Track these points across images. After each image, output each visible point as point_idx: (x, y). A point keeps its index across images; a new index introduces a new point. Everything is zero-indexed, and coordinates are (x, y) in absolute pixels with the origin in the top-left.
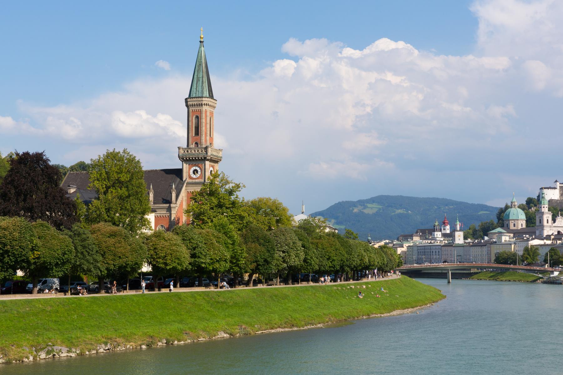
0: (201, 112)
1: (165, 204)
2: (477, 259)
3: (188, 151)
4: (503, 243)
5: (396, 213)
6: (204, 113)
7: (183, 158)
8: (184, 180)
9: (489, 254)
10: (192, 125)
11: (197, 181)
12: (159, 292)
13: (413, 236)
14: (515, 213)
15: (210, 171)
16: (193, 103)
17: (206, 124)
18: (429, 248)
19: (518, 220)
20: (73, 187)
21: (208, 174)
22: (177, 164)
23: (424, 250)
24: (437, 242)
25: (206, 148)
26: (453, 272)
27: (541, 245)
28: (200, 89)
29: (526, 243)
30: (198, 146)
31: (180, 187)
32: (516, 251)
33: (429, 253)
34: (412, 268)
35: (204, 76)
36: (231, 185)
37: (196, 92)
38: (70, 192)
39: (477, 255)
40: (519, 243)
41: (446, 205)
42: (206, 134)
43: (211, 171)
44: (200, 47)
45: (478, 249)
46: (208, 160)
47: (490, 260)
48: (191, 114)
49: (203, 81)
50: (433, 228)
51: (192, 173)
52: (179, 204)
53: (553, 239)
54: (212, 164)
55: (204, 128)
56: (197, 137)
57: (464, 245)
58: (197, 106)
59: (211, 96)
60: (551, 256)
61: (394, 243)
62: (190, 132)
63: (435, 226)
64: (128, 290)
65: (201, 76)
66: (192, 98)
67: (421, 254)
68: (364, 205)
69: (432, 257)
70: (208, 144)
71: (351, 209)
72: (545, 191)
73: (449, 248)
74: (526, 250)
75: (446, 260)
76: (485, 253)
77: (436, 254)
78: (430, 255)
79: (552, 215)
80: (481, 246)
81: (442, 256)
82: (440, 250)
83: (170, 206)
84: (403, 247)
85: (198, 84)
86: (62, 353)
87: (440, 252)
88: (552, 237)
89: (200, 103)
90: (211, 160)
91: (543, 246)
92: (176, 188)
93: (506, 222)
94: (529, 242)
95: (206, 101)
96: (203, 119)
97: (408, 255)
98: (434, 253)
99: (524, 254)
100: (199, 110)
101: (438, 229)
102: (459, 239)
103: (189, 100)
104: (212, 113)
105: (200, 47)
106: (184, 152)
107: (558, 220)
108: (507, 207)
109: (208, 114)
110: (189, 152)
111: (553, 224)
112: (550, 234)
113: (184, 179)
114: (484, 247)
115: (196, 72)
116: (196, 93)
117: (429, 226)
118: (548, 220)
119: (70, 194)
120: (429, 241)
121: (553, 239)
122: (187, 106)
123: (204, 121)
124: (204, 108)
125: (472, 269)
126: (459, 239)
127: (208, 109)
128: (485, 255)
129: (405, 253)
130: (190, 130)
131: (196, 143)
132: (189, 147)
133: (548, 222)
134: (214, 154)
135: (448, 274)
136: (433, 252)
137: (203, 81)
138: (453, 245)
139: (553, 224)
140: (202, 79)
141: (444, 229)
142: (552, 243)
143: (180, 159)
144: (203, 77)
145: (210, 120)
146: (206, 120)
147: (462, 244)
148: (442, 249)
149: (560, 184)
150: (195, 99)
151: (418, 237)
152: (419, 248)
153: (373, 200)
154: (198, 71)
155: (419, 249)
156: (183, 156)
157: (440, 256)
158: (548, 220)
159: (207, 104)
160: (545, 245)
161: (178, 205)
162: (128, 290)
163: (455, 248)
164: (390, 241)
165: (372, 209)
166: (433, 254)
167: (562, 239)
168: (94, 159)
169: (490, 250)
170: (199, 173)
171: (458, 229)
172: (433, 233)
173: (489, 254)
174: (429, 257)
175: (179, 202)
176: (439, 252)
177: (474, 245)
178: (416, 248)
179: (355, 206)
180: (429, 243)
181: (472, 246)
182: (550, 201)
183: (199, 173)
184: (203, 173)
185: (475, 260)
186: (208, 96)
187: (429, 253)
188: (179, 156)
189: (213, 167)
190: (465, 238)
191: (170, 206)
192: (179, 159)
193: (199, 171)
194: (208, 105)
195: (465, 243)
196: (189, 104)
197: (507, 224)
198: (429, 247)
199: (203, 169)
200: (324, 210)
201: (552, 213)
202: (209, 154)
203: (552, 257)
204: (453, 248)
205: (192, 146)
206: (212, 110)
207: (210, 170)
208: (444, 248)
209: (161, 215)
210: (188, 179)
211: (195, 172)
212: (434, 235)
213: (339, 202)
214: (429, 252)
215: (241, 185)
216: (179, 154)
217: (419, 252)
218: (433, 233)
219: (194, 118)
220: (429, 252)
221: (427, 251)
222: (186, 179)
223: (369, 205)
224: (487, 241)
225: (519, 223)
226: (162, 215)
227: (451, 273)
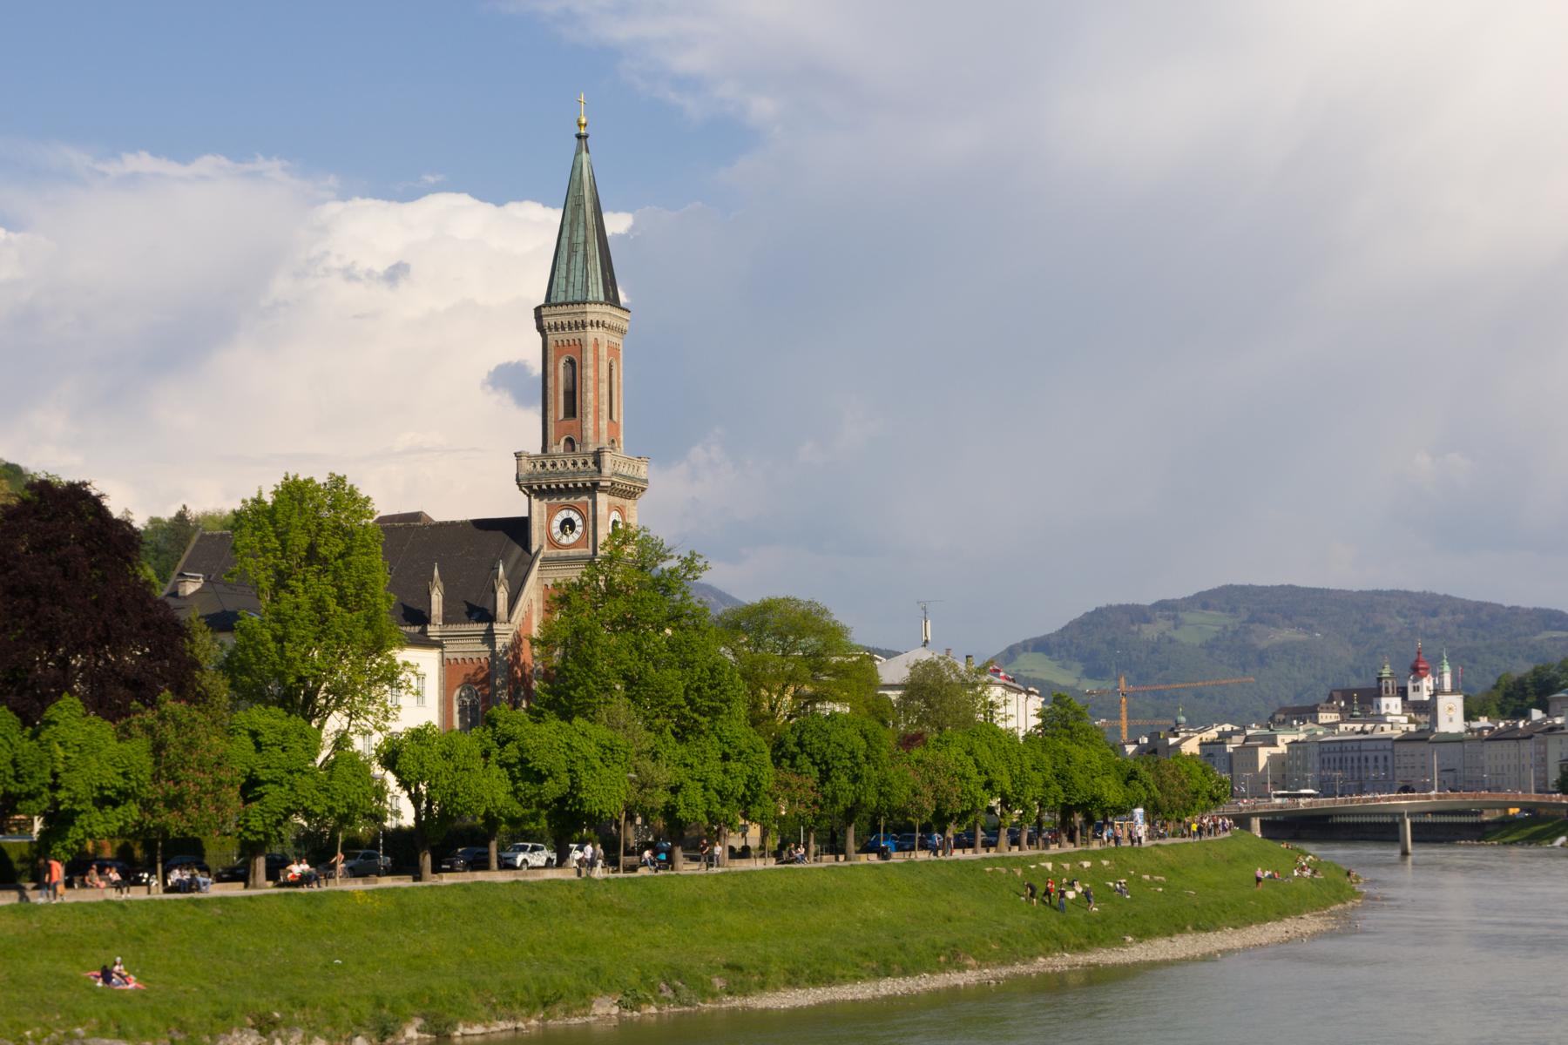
0: (580, 346)
1: (475, 625)
3: (544, 465)
6: (590, 348)
7: (530, 488)
8: (534, 550)
11: (571, 552)
12: (418, 884)
13: (1318, 712)
15: (610, 524)
16: (559, 320)
20: (192, 577)
21: (604, 532)
22: (513, 504)
24: (1382, 729)
25: (597, 457)
26: (1418, 819)
28: (579, 278)
30: (573, 450)
31: (522, 574)
34: (1325, 806)
35: (590, 240)
37: (567, 286)
38: (184, 592)
42: (597, 411)
43: (615, 523)
44: (578, 153)
45: (1509, 748)
46: (604, 490)
47: (1546, 784)
49: (585, 255)
50: (1373, 684)
51: (559, 530)
52: (518, 623)
54: (617, 501)
55: (591, 396)
56: (571, 422)
57: (1465, 736)
58: (570, 328)
59: (612, 299)
61: (1249, 732)
62: (551, 406)
63: (1380, 679)
65: (581, 239)
66: (556, 305)
67: (1332, 766)
69: (1364, 774)
70: (604, 441)
73: (1422, 747)
75: (1408, 784)
77: (1376, 767)
78: (1359, 768)
80: (1517, 739)
81: (1398, 772)
82: (1389, 754)
83: (490, 629)
84: (1275, 744)
85: (573, 262)
87: (1389, 759)
89: (579, 320)
90: (613, 490)
92: (509, 577)
95: (595, 312)
97: (1291, 770)
98: (1371, 763)
100: (577, 342)
101: (1390, 689)
102: (1451, 720)
103: (544, 311)
105: (578, 153)
106: (535, 466)
109: (603, 351)
113: (534, 549)
115: (566, 229)
116: (566, 291)
119: (185, 598)
120: (1358, 727)
122: (540, 328)
123: (590, 372)
124: (592, 334)
125: (1486, 812)
126: (1451, 720)
127: (603, 337)
129: (1283, 764)
130: (551, 400)
131: (570, 441)
132: (549, 452)
134: (624, 473)
135: (1401, 827)
136: (1367, 759)
137: (585, 255)
138: (1431, 738)
141: (1416, 689)
143: (521, 489)
144: (585, 243)
145: (611, 370)
146: (597, 371)
147: (1460, 734)
148: (1396, 750)
150: (564, 309)
151: (1333, 715)
152: (1326, 747)
153: (1203, 601)
154: (571, 225)
155: (1324, 752)
157: (1390, 773)
159: (601, 321)
163: (1438, 746)
164: (1235, 728)
165: (1196, 631)
166: (1366, 767)
169: (1546, 752)
170: (579, 529)
172: (1375, 700)
174: (1356, 775)
175: (520, 617)
176: (1386, 758)
178: (1316, 750)
179: (1148, 621)
180: (1358, 733)
181: (1488, 739)
183: (577, 529)
184: (590, 529)
186: (602, 298)
187: (1356, 764)
188: (518, 480)
189: (620, 510)
190: (1469, 715)
191: (492, 630)
192: (517, 487)
193: (578, 522)
194: (603, 325)
195: (1472, 730)
196: (545, 324)
198: (1356, 746)
199: (590, 518)
200: (1052, 634)
202: (606, 471)
204: (1431, 745)
205: (558, 449)
206: (615, 340)
207: (612, 520)
208: (1398, 747)
209: (459, 656)
210: (545, 546)
211: (568, 525)
212: (1379, 707)
214: (1356, 761)
215: (700, 563)
216: (517, 475)
217: (1326, 760)
218: (1375, 700)
219: (561, 365)
220: (1356, 761)
224: (1537, 724)
226: (468, 655)
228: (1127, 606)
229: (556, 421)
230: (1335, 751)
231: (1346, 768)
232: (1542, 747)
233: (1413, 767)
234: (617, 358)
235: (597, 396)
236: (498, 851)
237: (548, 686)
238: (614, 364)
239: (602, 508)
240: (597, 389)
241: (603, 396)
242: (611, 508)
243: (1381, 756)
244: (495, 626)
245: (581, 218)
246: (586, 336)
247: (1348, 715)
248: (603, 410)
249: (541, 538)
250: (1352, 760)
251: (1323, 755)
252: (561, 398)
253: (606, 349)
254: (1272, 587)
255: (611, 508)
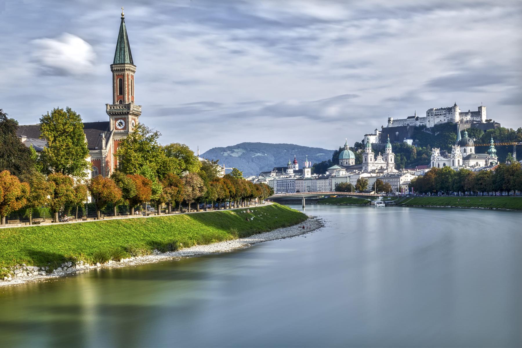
0: (123, 76)
2: (322, 189)
3: (114, 108)
4: (341, 176)
5: (256, 155)
6: (126, 76)
7: (110, 113)
8: (111, 131)
9: (330, 184)
10: (117, 86)
14: (347, 154)
15: (132, 124)
17: (128, 85)
18: (286, 182)
19: (349, 159)
20: (23, 137)
22: (106, 118)
23: (282, 183)
27: (369, 177)
28: (123, 57)
29: (358, 176)
32: (350, 182)
33: (286, 186)
35: (126, 47)
36: (150, 134)
37: (119, 59)
39: (322, 186)
40: (353, 176)
41: (293, 149)
42: (128, 93)
45: (323, 181)
46: (131, 114)
48: (116, 77)
53: (377, 173)
54: (134, 117)
55: (126, 89)
56: (122, 96)
57: (312, 178)
59: (132, 63)
60: (377, 186)
61: (259, 178)
63: (288, 165)
64: (77, 219)
65: (123, 46)
66: (117, 64)
67: (280, 186)
68: (232, 150)
70: (130, 101)
71: (222, 153)
72: (369, 137)
73: (301, 181)
74: (359, 181)
75: (299, 190)
76: (327, 184)
77: (291, 186)
79: (374, 155)
81: (296, 187)
82: (294, 183)
86: (34, 271)
88: (377, 171)
90: (133, 114)
91: (370, 178)
92: (105, 137)
93: (340, 161)
94: (360, 175)
96: (125, 81)
98: (290, 185)
99: (357, 184)
102: (308, 174)
104: (132, 76)
107: (379, 158)
108: (341, 150)
109: (130, 77)
110: (115, 108)
111: (375, 162)
112: (375, 169)
114: (327, 180)
116: (119, 61)
117: (283, 165)
118: (391, 159)
121: (377, 173)
126: (308, 174)
128: (327, 186)
132: (115, 104)
133: (371, 161)
135: (303, 200)
136: (288, 184)
139: (375, 162)
140: (124, 49)
142: (377, 175)
144: (124, 47)
145: (131, 82)
146: (128, 82)
149: (379, 131)
150: (119, 66)
154: (120, 43)
156: (110, 111)
158: (391, 159)
160: (372, 177)
161: (107, 151)
162: (77, 219)
163: (306, 181)
164: (256, 177)
167: (383, 172)
168: (44, 115)
169: (332, 182)
171: (307, 167)
172: (287, 170)
173: (330, 184)
176: (293, 184)
177: (320, 178)
180: (285, 178)
182: (372, 144)
183: (123, 125)
185: (320, 189)
186: (129, 63)
187: (286, 186)
188: (107, 111)
189: (134, 120)
190: (312, 174)
191: (102, 152)
192: (106, 113)
197: (341, 162)
201: (374, 153)
203: (378, 186)
204: (304, 181)
206: (132, 74)
208: (297, 181)
210: (114, 129)
212: (288, 172)
213: (213, 148)
214: (286, 185)
215: (159, 134)
216: (107, 110)
219: (118, 80)
220: (286, 185)
221: (284, 183)
222: (113, 129)
223: (235, 150)
225: (350, 161)
227: (305, 200)
228: (220, 147)
229: (117, 96)
230: (281, 182)
231: (283, 187)
232: (331, 181)
233: (300, 186)
234: (133, 79)
235: (128, 89)
236: (166, 214)
237: (332, 161)
238: (132, 80)
239: (130, 119)
240: (128, 87)
241: (130, 89)
242: (132, 119)
243: (292, 183)
244: (102, 151)
245: (123, 41)
246: (125, 73)
247: (281, 174)
248: (130, 93)
249: (113, 127)
250: (285, 184)
251: (278, 183)
252: (118, 89)
253: (130, 76)
254: (255, 143)
255: (132, 119)
